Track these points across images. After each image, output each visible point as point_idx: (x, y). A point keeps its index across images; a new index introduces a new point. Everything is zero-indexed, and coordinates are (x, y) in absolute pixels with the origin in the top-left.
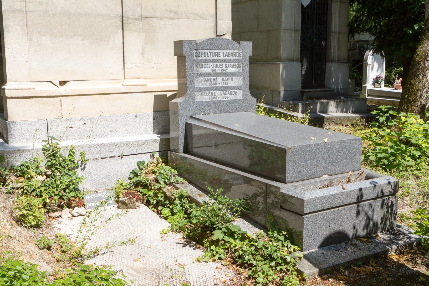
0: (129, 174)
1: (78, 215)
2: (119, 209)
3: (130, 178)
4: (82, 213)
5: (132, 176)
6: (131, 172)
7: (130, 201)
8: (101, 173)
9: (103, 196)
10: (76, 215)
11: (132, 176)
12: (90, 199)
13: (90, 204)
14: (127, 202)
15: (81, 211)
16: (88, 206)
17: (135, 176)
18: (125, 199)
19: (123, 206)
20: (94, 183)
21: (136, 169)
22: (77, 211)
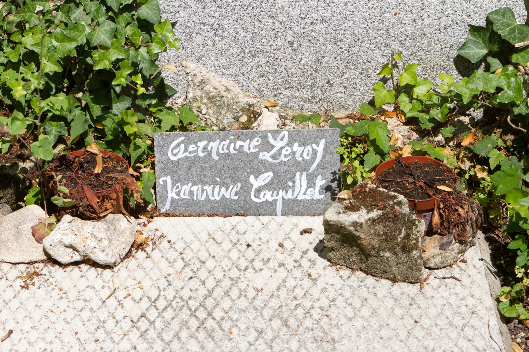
0: (461, 34)
1: (77, 257)
2: (322, 262)
3: (465, 66)
4: (100, 257)
5: (477, 51)
6: (474, 30)
7: (388, 238)
8: (295, 13)
9: (265, 156)
10: (65, 256)
11: (477, 51)
12: (192, 161)
13: (186, 188)
14: (365, 237)
15: (92, 243)
16: (171, 195)
17: (491, 54)
18: (355, 224)
19: (344, 251)
20: (252, 62)
21: (507, 12)
22: (68, 241)
